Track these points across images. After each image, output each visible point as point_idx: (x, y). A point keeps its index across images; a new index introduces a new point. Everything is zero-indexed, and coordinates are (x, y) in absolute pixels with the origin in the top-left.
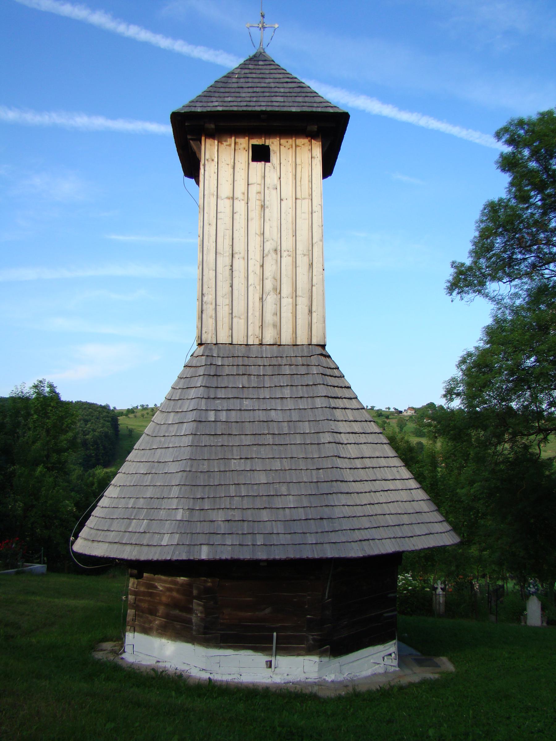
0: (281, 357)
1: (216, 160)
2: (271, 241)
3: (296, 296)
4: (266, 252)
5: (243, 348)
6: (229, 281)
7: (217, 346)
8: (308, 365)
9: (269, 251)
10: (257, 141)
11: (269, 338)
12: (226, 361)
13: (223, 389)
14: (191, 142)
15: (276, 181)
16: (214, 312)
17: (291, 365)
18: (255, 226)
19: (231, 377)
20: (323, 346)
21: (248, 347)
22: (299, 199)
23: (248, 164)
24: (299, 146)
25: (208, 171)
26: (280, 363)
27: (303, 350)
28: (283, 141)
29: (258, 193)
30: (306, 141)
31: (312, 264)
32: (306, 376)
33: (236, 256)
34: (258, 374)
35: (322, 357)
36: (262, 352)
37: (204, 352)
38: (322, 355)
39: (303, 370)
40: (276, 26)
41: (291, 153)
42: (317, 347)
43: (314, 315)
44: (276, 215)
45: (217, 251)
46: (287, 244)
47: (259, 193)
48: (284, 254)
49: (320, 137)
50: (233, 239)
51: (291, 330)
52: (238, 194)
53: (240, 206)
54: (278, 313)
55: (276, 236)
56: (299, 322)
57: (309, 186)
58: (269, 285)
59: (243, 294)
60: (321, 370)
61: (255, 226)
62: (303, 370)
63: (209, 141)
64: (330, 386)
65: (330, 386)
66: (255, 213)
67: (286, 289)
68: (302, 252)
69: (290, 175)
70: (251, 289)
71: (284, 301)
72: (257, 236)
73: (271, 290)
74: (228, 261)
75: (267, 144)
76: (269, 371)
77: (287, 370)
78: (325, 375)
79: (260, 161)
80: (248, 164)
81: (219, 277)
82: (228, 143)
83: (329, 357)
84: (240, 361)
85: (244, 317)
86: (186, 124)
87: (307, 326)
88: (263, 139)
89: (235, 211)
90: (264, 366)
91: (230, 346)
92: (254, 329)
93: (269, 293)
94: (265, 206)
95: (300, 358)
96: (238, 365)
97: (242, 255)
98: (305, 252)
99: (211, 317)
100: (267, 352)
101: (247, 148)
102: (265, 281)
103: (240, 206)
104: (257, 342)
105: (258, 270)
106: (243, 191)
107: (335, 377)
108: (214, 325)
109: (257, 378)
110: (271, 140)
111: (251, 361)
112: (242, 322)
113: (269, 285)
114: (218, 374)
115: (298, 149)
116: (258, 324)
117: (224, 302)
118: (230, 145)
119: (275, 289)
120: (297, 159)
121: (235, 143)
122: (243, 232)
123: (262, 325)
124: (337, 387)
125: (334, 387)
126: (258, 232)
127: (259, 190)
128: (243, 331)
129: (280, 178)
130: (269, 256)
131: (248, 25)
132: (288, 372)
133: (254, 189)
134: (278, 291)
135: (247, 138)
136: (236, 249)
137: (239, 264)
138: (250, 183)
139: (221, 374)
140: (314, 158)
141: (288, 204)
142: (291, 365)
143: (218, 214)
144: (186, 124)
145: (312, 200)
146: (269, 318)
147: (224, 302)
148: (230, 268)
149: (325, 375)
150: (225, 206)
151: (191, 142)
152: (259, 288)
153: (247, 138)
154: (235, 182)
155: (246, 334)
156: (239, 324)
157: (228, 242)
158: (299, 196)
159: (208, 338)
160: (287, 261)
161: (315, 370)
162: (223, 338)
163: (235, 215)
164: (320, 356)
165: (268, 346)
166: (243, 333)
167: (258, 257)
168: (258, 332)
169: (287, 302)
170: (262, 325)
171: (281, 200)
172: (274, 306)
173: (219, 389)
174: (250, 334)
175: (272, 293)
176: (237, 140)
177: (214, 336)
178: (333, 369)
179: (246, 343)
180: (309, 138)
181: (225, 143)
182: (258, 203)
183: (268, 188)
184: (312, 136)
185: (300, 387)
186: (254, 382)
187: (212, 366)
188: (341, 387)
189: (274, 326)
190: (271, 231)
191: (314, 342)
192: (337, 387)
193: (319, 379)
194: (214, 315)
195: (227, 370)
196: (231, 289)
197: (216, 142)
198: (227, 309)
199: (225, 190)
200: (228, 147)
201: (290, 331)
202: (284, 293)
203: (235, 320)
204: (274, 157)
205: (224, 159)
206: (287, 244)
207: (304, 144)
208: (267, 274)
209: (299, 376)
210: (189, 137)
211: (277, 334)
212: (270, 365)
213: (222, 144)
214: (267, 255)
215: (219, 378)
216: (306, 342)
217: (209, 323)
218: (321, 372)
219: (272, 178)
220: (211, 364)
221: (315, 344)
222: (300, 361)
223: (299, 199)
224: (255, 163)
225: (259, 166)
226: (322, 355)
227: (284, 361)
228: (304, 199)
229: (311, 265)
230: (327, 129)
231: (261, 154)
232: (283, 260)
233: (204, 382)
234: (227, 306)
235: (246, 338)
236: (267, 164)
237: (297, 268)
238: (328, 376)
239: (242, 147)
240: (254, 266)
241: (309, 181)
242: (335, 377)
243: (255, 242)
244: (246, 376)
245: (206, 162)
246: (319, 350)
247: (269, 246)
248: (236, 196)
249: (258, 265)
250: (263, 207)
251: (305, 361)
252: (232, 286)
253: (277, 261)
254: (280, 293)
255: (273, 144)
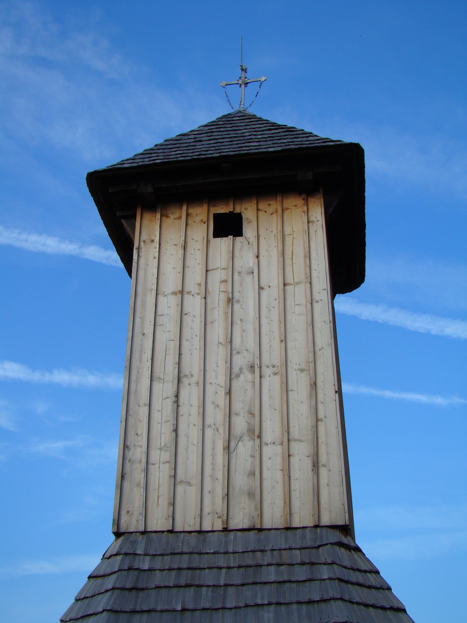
0: (262, 551)
1: (157, 239)
2: (245, 352)
3: (289, 440)
4: (236, 370)
5: (193, 540)
6: (173, 421)
7: (145, 536)
8: (312, 564)
9: (241, 369)
10: (222, 209)
11: (240, 520)
12: (158, 563)
13: (145, 616)
14: (123, 221)
15: (251, 262)
16: (143, 475)
17: (279, 565)
18: (218, 332)
19: (164, 591)
20: (347, 529)
21: (202, 537)
22: (290, 284)
23: (208, 241)
24: (287, 209)
25: (146, 256)
26: (259, 562)
27: (303, 537)
28: (262, 206)
29: (223, 281)
30: (299, 201)
31: (315, 383)
32: (307, 584)
33: (185, 381)
34: (216, 583)
35: (343, 550)
36: (226, 542)
37: (121, 548)
38: (341, 544)
39: (301, 573)
40: (263, 79)
41: (275, 221)
42: (331, 531)
43: (323, 472)
44: (251, 313)
45: (154, 375)
46: (272, 355)
47: (225, 281)
48: (267, 372)
49: (321, 191)
50: (180, 354)
51: (282, 502)
52: (191, 286)
53: (194, 304)
54: (257, 473)
55: (251, 343)
56: (295, 485)
57: (305, 262)
58: (240, 424)
59: (195, 442)
60: (338, 572)
61: (218, 332)
62: (301, 573)
63: (147, 217)
64: (358, 603)
65: (358, 603)
66: (218, 315)
67: (272, 430)
68: (297, 367)
69: (275, 250)
70: (209, 433)
71: (268, 451)
72: (221, 347)
73: (245, 432)
74: (170, 389)
75: (237, 211)
76: (237, 577)
77: (271, 574)
78: (347, 582)
79: (226, 236)
80: (208, 241)
81: (156, 416)
82: (176, 216)
83: (358, 549)
84: (184, 561)
85: (196, 481)
86: (110, 191)
87: (311, 490)
88: (231, 204)
89: (186, 311)
90: (229, 568)
91: (170, 535)
92: (214, 502)
93: (241, 437)
94: (235, 300)
95: (298, 552)
96: (179, 569)
97: (194, 380)
98: (303, 366)
99: (138, 485)
100: (237, 543)
101: (205, 219)
102: (234, 418)
103: (194, 304)
104: (219, 526)
105: (222, 400)
106: (199, 281)
107: (370, 587)
108: (143, 498)
109: (213, 592)
110: (245, 205)
111: (205, 561)
112: (193, 492)
113: (240, 424)
114: (140, 585)
115: (286, 213)
116: (220, 491)
117: (160, 457)
118: (180, 218)
119: (251, 431)
120: (294, 235)
121: (188, 215)
122: (197, 343)
123: (228, 495)
124: (373, 606)
125: (367, 606)
126: (222, 340)
127: (224, 278)
128: (196, 507)
129: (258, 257)
130: (242, 377)
131: (224, 84)
132: (272, 578)
133: (216, 277)
134: (257, 432)
135: (205, 206)
136: (186, 370)
137: (191, 395)
138: (210, 267)
139: (144, 586)
140: (313, 222)
141: (271, 296)
142: (279, 565)
143: (158, 318)
144: (110, 191)
145: (310, 283)
146: (240, 480)
147: (160, 457)
148: (174, 399)
149: (347, 582)
150: (169, 305)
151: (123, 221)
152: (223, 431)
153: (205, 206)
154: (187, 270)
155: (198, 512)
156: (187, 497)
157: (172, 359)
158: (289, 279)
159: (132, 523)
160: (272, 383)
161: (325, 572)
162: (158, 522)
163: (185, 317)
164: (337, 548)
165: (239, 533)
166: (193, 511)
167: (222, 379)
168: (220, 506)
169: (273, 454)
170: (228, 495)
171: (261, 288)
172: (250, 460)
173: (137, 616)
174: (207, 509)
175: (246, 438)
176: (191, 211)
177: (142, 518)
178: (365, 572)
179: (198, 529)
180: (304, 196)
181: (172, 217)
182: (223, 297)
183: (239, 273)
184: (306, 191)
185: (295, 606)
186: (206, 598)
187: (131, 572)
188: (383, 608)
189: (251, 495)
190: (246, 338)
191: (326, 520)
192: (373, 606)
193: (333, 590)
194: (143, 481)
195: (158, 579)
196: (174, 434)
197: (158, 216)
198: (166, 470)
199: (171, 282)
200: (177, 221)
201: (280, 503)
202: (268, 436)
203: (180, 489)
204: (249, 231)
205: (174, 244)
206: (272, 355)
207: (295, 206)
208: (238, 406)
209: (294, 585)
210: (119, 214)
211: (256, 509)
212: (239, 567)
213: (167, 217)
214: (238, 376)
215: (141, 594)
216: (310, 523)
217: (135, 497)
218: (338, 575)
219: (245, 258)
220: (130, 569)
221: (328, 524)
222: (297, 556)
223: (290, 284)
224: (218, 239)
225: (223, 244)
226: (341, 544)
227: (267, 558)
228: (298, 284)
229: (314, 385)
230: (330, 178)
231: (228, 227)
232: (266, 382)
233: (112, 601)
234: (167, 465)
235: (198, 520)
236: (238, 239)
237: (290, 393)
238: (353, 584)
239: (198, 219)
240: (217, 395)
241: (305, 257)
242: (370, 587)
243: (218, 356)
244: (192, 589)
245: (142, 244)
246: (337, 536)
247: (240, 361)
248: (187, 289)
249: (222, 392)
250: (230, 301)
251: (306, 556)
252: (176, 430)
253: (254, 382)
254: (260, 437)
255: (248, 211)
